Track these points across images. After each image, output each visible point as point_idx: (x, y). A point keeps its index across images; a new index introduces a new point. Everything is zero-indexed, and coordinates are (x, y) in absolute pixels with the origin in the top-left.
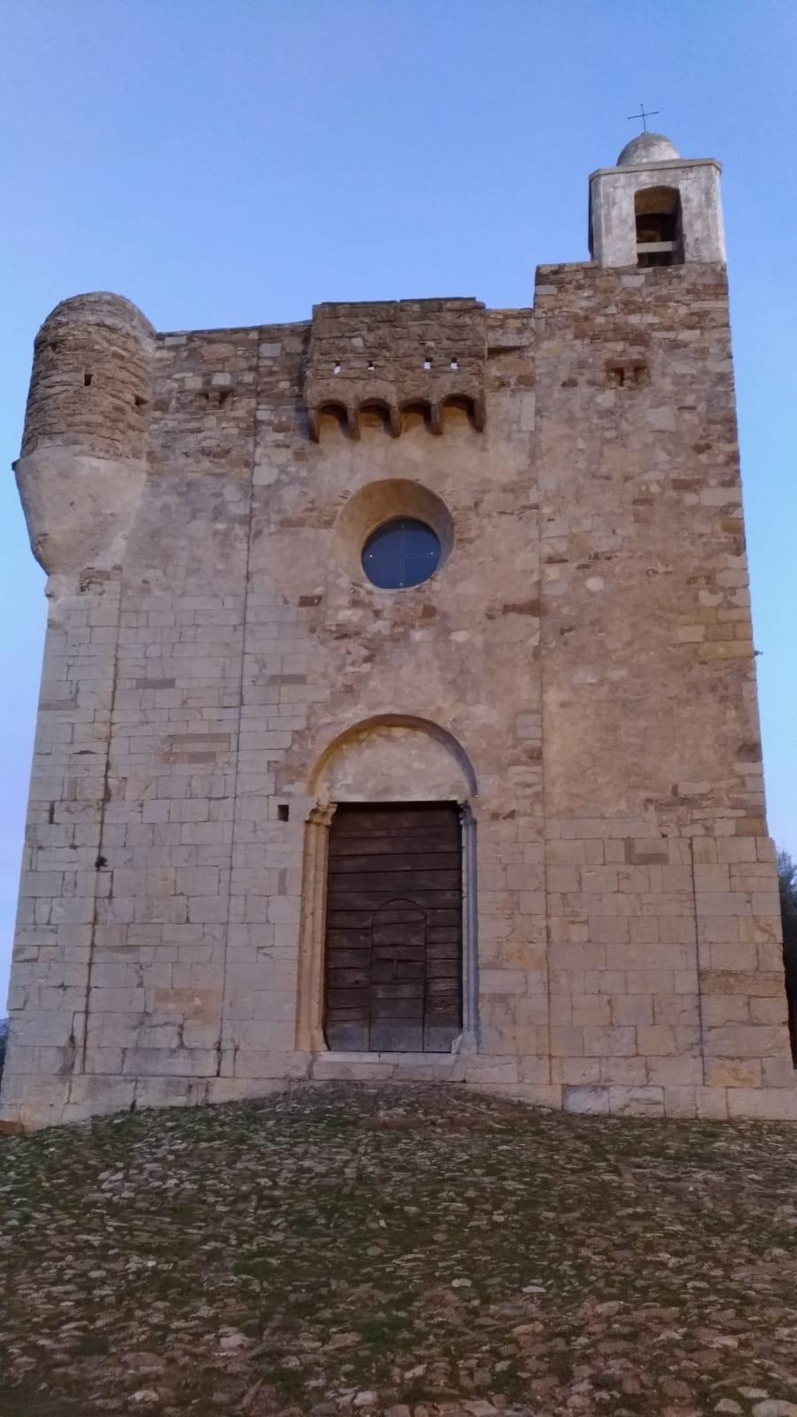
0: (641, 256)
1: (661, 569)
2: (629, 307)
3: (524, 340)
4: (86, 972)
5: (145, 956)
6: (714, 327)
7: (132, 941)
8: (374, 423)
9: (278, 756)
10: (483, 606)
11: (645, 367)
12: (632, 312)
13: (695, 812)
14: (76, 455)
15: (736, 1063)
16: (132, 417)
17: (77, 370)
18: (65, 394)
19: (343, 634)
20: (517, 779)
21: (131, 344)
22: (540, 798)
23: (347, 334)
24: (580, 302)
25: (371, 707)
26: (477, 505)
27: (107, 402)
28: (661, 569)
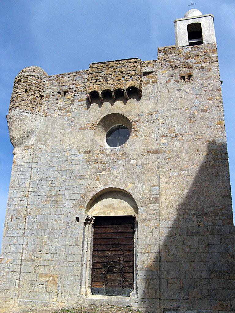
0: (189, 43)
1: (198, 137)
2: (187, 58)
3: (154, 69)
4: (20, 266)
5: (37, 263)
6: (213, 62)
7: (33, 258)
8: (108, 97)
9: (77, 202)
10: (141, 152)
11: (192, 75)
12: (188, 59)
13: (209, 217)
14: (21, 112)
15: (222, 302)
16: (38, 100)
17: (23, 89)
18: (20, 95)
19: (97, 162)
20: (151, 208)
21: (39, 80)
22: (159, 214)
23: (99, 72)
24: (171, 57)
25: (105, 185)
26: (139, 120)
27: (31, 97)
28: (198, 137)
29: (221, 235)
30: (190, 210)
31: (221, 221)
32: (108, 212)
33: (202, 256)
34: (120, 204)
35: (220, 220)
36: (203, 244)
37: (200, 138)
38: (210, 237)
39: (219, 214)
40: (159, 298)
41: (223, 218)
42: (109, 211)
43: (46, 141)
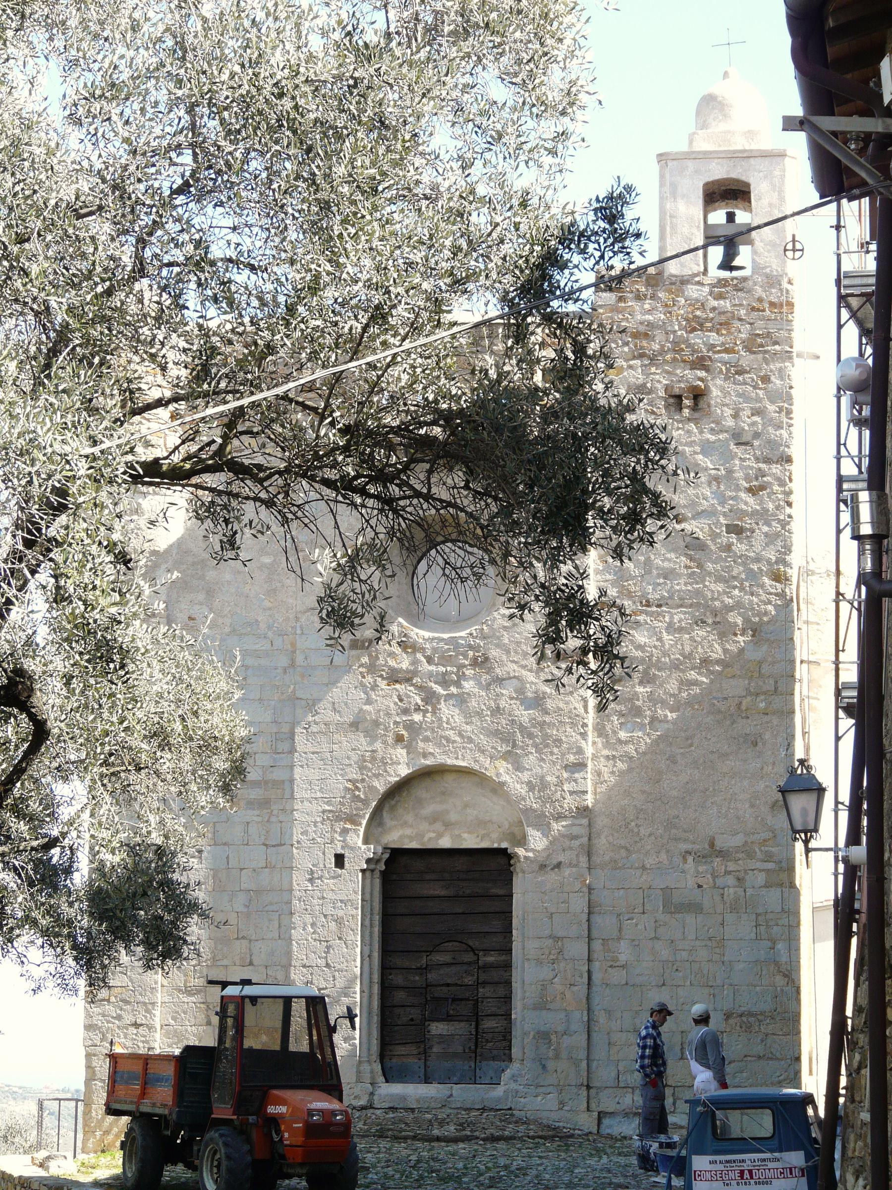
2: (695, 325)
29: (758, 915)
30: (677, 840)
31: (763, 874)
32: (433, 835)
33: (705, 972)
34: (468, 811)
35: (760, 871)
36: (710, 939)
37: (718, 620)
38: (730, 918)
39: (759, 855)
40: (592, 1091)
41: (770, 866)
42: (434, 831)
43: (210, 593)
